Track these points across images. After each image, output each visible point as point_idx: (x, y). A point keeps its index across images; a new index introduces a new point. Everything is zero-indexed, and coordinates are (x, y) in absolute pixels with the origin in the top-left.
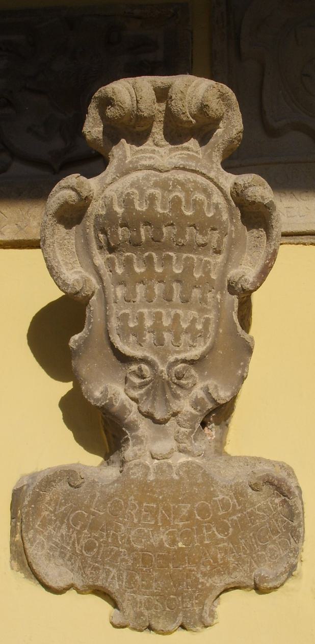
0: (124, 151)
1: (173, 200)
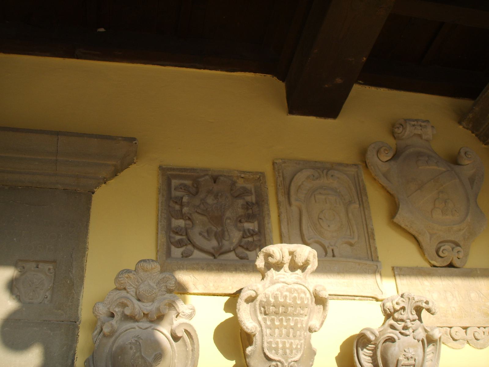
0: (272, 273)
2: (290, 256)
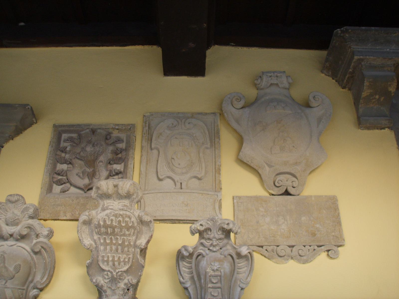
1: (118, 221)
2: (115, 188)
